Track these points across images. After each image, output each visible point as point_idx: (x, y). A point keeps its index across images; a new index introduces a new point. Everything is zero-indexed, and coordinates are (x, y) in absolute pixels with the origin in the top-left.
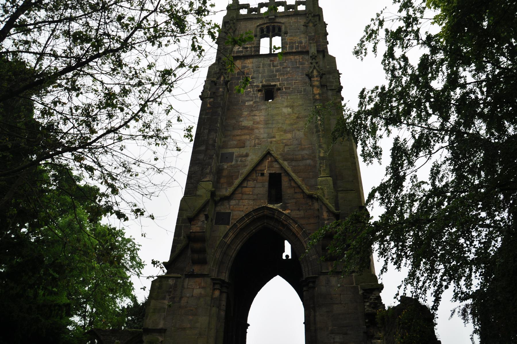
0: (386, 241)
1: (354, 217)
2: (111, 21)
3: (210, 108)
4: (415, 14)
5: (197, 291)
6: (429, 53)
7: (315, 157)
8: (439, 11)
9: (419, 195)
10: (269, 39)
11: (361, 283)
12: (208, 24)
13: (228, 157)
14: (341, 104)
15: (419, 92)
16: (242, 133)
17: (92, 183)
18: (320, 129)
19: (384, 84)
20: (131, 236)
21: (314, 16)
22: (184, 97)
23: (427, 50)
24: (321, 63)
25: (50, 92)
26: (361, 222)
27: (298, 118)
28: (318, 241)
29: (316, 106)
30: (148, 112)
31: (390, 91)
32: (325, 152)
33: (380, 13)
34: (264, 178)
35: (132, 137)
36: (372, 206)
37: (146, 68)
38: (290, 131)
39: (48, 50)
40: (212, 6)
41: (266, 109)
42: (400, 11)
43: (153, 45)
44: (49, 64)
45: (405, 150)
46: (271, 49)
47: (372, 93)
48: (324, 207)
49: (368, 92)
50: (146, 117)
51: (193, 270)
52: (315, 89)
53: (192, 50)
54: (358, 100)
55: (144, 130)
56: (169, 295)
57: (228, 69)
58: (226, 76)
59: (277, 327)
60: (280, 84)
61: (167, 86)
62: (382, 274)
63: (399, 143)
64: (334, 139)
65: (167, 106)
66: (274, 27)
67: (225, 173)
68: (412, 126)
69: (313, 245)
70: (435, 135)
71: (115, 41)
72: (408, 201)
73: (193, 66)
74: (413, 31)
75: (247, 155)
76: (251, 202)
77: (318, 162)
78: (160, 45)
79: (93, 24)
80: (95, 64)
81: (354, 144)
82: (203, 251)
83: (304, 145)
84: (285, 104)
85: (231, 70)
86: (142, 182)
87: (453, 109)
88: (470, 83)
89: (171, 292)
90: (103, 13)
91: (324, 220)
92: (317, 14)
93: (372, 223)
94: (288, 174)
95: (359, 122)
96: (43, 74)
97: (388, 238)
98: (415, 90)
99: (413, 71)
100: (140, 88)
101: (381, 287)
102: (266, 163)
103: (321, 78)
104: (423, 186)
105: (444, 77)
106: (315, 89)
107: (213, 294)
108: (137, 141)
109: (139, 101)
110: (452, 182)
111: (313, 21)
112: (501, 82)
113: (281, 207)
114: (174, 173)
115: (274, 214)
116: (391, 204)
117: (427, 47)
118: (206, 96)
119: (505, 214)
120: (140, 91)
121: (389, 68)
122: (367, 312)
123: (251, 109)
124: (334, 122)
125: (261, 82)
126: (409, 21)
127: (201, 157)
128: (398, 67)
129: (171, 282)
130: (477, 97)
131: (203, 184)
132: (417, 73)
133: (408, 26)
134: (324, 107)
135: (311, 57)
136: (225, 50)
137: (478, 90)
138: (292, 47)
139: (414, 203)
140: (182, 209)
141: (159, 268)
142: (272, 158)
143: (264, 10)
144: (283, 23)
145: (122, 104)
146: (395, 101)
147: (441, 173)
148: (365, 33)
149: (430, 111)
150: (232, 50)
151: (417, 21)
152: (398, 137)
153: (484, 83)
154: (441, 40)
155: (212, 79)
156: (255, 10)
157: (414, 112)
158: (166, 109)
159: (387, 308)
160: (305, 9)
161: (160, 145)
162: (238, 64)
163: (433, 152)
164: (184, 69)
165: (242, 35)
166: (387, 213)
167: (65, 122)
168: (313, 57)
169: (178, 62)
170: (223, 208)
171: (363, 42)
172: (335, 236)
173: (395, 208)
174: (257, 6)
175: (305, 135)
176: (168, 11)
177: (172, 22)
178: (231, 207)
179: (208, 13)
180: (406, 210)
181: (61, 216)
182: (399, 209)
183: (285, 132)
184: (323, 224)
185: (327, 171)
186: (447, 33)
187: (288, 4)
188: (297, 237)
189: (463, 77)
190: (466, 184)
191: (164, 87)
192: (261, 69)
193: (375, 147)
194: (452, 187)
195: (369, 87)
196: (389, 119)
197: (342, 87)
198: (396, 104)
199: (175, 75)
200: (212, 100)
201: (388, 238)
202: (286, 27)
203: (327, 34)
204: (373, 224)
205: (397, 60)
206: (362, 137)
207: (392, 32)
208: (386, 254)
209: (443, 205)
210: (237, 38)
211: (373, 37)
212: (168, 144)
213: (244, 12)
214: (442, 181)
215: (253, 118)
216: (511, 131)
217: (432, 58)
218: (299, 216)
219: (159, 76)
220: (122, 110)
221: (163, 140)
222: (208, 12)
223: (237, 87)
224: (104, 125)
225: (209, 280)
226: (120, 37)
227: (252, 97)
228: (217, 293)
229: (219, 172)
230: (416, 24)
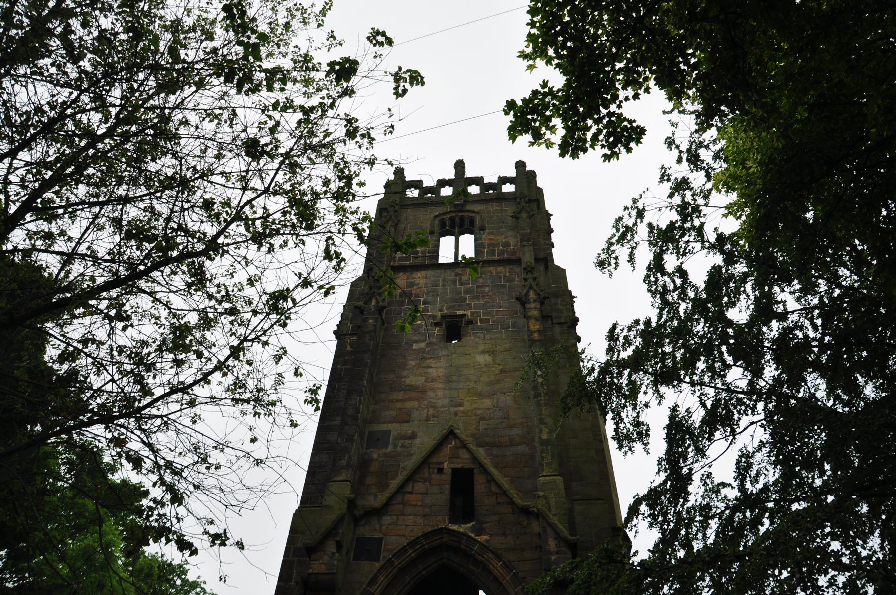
2: (192, 207)
4: (695, 200)
6: (722, 264)
8: (733, 197)
9: (717, 508)
10: (453, 238)
12: (352, 213)
13: (379, 440)
14: (577, 349)
15: (709, 328)
16: (407, 397)
17: (135, 478)
19: (649, 316)
20: (199, 577)
21: (530, 201)
23: (718, 259)
24: (541, 279)
25: (78, 318)
26: (617, 562)
27: (502, 371)
29: (533, 353)
31: (659, 326)
33: (638, 197)
35: (213, 400)
36: (634, 529)
37: (245, 284)
39: (82, 249)
40: (361, 184)
41: (448, 356)
42: (671, 196)
44: (82, 270)
45: (689, 428)
47: (629, 331)
48: (549, 530)
49: (622, 330)
50: (241, 369)
53: (324, 258)
60: (472, 314)
63: (678, 416)
64: (565, 409)
65: (278, 349)
66: (462, 219)
67: (374, 467)
68: (699, 387)
70: (740, 402)
71: (195, 240)
72: (698, 518)
74: (693, 228)
75: (413, 436)
76: (419, 520)
77: (539, 449)
78: (271, 250)
79: (162, 208)
80: (160, 273)
84: (481, 348)
85: (390, 293)
86: (226, 483)
87: (768, 357)
88: (793, 312)
90: (180, 194)
94: (486, 471)
95: (608, 380)
96: (70, 287)
98: (702, 324)
99: (696, 294)
102: (447, 451)
103: (542, 304)
104: (724, 491)
105: (749, 303)
108: (221, 407)
110: (775, 483)
112: (845, 309)
113: (473, 529)
114: (284, 467)
116: (668, 525)
117: (718, 254)
119: (874, 541)
120: (232, 323)
123: (422, 356)
124: (564, 380)
125: (441, 310)
126: (687, 211)
127: (333, 437)
128: (672, 286)
130: (806, 337)
131: (333, 487)
132: (704, 296)
133: (684, 221)
135: (524, 269)
137: (807, 323)
138: (492, 253)
139: (710, 521)
142: (458, 441)
143: (447, 191)
144: (478, 213)
145: (200, 343)
146: (669, 343)
147: (755, 467)
148: (614, 230)
149: (729, 360)
151: (700, 212)
152: (677, 406)
153: (817, 312)
154: (742, 243)
155: (357, 304)
156: (430, 189)
157: (702, 362)
160: (513, 190)
161: (262, 416)
162: (402, 280)
163: (738, 431)
165: (409, 236)
166: (661, 541)
167: (98, 370)
168: (528, 270)
169: (300, 278)
170: (367, 531)
171: (611, 244)
173: (677, 530)
176: (286, 192)
177: (293, 213)
178: (384, 528)
179: (354, 198)
180: (697, 534)
181: (72, 537)
182: (683, 532)
183: (481, 395)
186: (749, 232)
187: (486, 181)
189: (781, 302)
190: (800, 485)
193: (637, 424)
194: (776, 492)
195: (624, 321)
196: (659, 375)
202: (482, 220)
203: (552, 231)
204: (639, 564)
205: (669, 275)
209: (762, 525)
210: (401, 241)
211: (629, 238)
213: (413, 193)
214: (757, 481)
215: (426, 370)
216: (869, 391)
217: (727, 271)
220: (199, 355)
222: (354, 196)
224: (165, 379)
226: (204, 234)
227: (425, 335)
229: (364, 464)
230: (698, 217)
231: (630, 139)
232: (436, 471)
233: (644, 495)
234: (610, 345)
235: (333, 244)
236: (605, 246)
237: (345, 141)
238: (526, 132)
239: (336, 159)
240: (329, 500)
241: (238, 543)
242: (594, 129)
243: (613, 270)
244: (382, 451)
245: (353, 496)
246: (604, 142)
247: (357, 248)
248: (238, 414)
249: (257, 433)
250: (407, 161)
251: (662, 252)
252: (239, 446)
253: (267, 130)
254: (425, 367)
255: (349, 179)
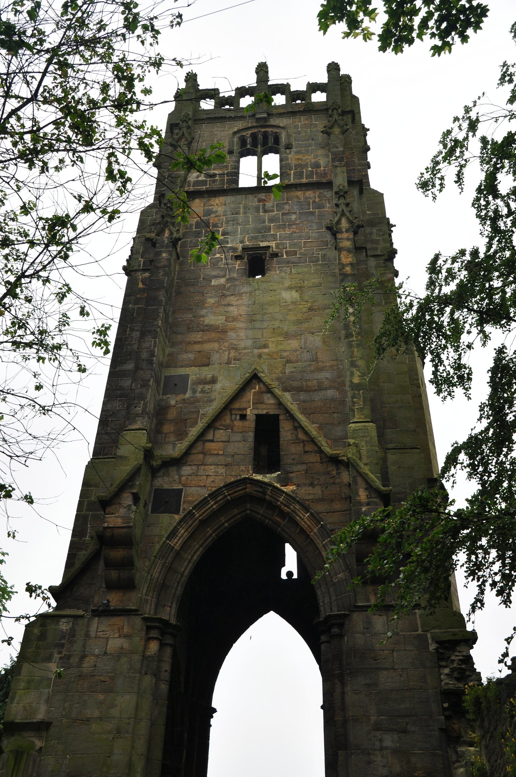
0: (481, 547)
1: (417, 501)
3: (142, 290)
5: (115, 644)
7: (343, 384)
10: (255, 158)
11: (433, 628)
12: (138, 128)
13: (177, 385)
16: (205, 338)
18: (354, 330)
19: (477, 245)
22: (92, 270)
24: (355, 206)
26: (431, 511)
27: (310, 309)
28: (349, 546)
29: (345, 288)
30: (22, 296)
31: (488, 257)
32: (363, 375)
33: (471, 105)
34: (246, 423)
36: (452, 479)
37: (18, 212)
38: (296, 335)
40: (147, 92)
43: (30, 168)
46: (259, 178)
47: (453, 263)
48: (360, 480)
49: (445, 262)
50: (19, 308)
51: (109, 601)
52: (344, 254)
54: (426, 277)
55: (15, 332)
56: (60, 653)
57: (178, 215)
58: (173, 229)
59: (269, 690)
60: (277, 246)
61: (59, 248)
62: (474, 611)
64: (379, 350)
65: (60, 286)
66: (265, 135)
67: (172, 414)
69: (338, 554)
73: (110, 209)
75: (213, 381)
76: (221, 470)
77: (350, 394)
81: (418, 360)
82: (128, 564)
83: (323, 362)
84: (287, 283)
85: (183, 218)
89: (62, 645)
91: (361, 504)
92: (348, 109)
93: (452, 513)
94: (292, 417)
95: (428, 317)
97: (484, 541)
100: (7, 251)
101: (472, 638)
102: (250, 395)
103: (355, 233)
106: (344, 254)
107: (146, 647)
109: (5, 276)
111: (341, 123)
113: (279, 479)
115: (265, 493)
116: (489, 476)
118: (136, 268)
120: (6, 257)
121: (486, 215)
122: (446, 687)
123: (222, 293)
125: (242, 242)
127: (126, 383)
128: (505, 211)
129: (64, 626)
131: (128, 436)
134: (361, 290)
135: (336, 193)
136: (173, 179)
138: (300, 175)
140: (87, 484)
141: (39, 599)
142: (262, 385)
143: (246, 101)
144: (283, 128)
146: (498, 277)
148: (441, 147)
150: (186, 178)
152: (504, 347)
155: (148, 235)
158: (57, 291)
159: (484, 681)
160: (324, 99)
161: (46, 361)
162: (198, 206)
164: (92, 217)
165: (204, 151)
166: (481, 493)
168: (341, 194)
170: (167, 482)
171: (437, 163)
172: (383, 537)
173: (498, 483)
174: (233, 94)
175: (324, 342)
176: (59, 100)
177: (67, 124)
178: (183, 478)
182: (505, 485)
183: (287, 336)
184: (359, 513)
185: (367, 412)
187: (293, 89)
188: (308, 536)
191: (54, 249)
192: (241, 217)
193: (458, 366)
195: (448, 251)
196: (485, 313)
197: (395, 252)
198: (500, 284)
199: (74, 228)
200: (147, 274)
201: (484, 541)
202: (288, 136)
203: (368, 149)
204: (456, 514)
205: (502, 198)
206: (433, 346)
207: (494, 143)
208: (480, 574)
210: (194, 157)
211: (458, 154)
212: (61, 359)
213: (207, 105)
218: (311, 497)
219: (43, 229)
221: (52, 351)
223: (195, 251)
225: (138, 621)
228: (154, 647)
229: (161, 412)
231: (467, 24)
232: (238, 417)
233: (464, 443)
234: (431, 277)
235: (117, 161)
236: (430, 165)
237: (123, 35)
238: (340, 19)
239: (115, 59)
240: (124, 450)
241: (26, 497)
242: (423, 13)
243: (437, 193)
244: (180, 397)
245: (150, 445)
246: (434, 30)
247: (146, 168)
248: (20, 359)
249: (42, 380)
250: (199, 61)
251: (496, 170)
252: (23, 393)
253: (25, 14)
254: (225, 305)
255: (130, 80)
